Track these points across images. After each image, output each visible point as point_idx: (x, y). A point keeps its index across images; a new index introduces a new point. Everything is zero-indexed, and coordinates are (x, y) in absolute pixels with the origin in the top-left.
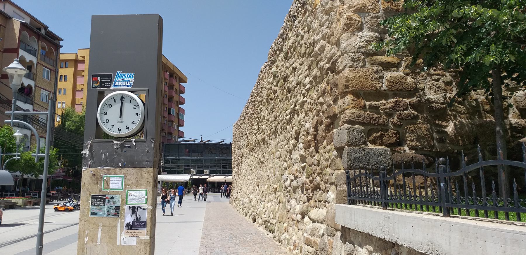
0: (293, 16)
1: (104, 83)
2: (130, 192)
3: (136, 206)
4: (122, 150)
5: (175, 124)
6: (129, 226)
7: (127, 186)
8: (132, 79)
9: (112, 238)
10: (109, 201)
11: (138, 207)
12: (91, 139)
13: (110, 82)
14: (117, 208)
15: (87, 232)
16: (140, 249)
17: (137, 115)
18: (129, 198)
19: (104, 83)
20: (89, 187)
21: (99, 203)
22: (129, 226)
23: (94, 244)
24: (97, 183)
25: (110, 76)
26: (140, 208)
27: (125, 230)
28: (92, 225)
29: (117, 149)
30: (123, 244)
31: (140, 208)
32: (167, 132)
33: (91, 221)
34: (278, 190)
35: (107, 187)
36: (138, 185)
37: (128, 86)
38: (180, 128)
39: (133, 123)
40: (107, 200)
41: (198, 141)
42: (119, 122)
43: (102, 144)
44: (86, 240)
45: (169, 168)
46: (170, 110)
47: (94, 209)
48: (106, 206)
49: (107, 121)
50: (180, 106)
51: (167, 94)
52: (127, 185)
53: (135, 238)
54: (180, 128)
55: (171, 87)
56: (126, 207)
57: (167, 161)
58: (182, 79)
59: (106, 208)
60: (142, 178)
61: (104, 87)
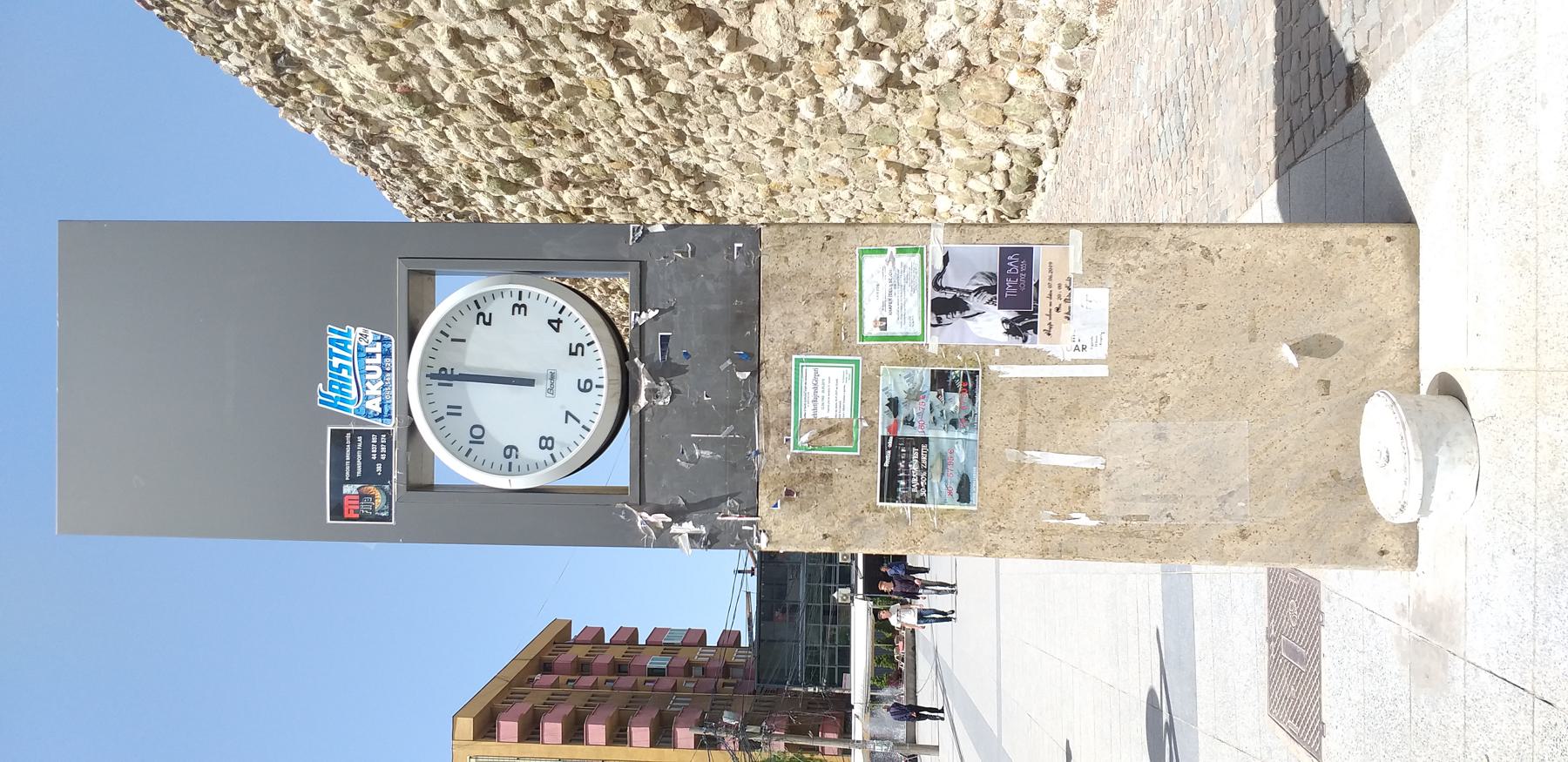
0: (278, 72)
1: (368, 464)
2: (870, 329)
3: (933, 294)
4: (680, 370)
5: (698, 656)
6: (1022, 326)
7: (841, 342)
8: (356, 333)
9: (1076, 400)
10: (909, 422)
11: (937, 287)
12: (629, 514)
13: (367, 435)
14: (941, 381)
15: (1047, 518)
16: (1129, 268)
17: (520, 307)
18: (894, 328)
19: (368, 464)
20: (845, 512)
21: (914, 467)
22: (1022, 326)
23: (1101, 481)
24: (826, 477)
25: (338, 436)
26: (940, 275)
27: (1038, 342)
28: (1015, 495)
29: (675, 392)
30: (1101, 352)
31: (940, 275)
32: (721, 681)
33: (994, 502)
34: (892, 156)
35: (842, 434)
36: (837, 292)
37: (386, 354)
38: (712, 641)
39: (555, 324)
40: (905, 431)
41: (752, 583)
42: (551, 390)
43: (648, 464)
44: (1083, 521)
45: (832, 671)
46: (652, 672)
47: (940, 487)
48: (930, 434)
49: (546, 443)
50: (642, 641)
51: (602, 679)
52: (837, 340)
53: (1079, 294)
54: (712, 641)
55: (582, 668)
56: (933, 342)
57: (808, 674)
58: (561, 636)
59: (940, 435)
60: (808, 275)
61: (387, 465)
